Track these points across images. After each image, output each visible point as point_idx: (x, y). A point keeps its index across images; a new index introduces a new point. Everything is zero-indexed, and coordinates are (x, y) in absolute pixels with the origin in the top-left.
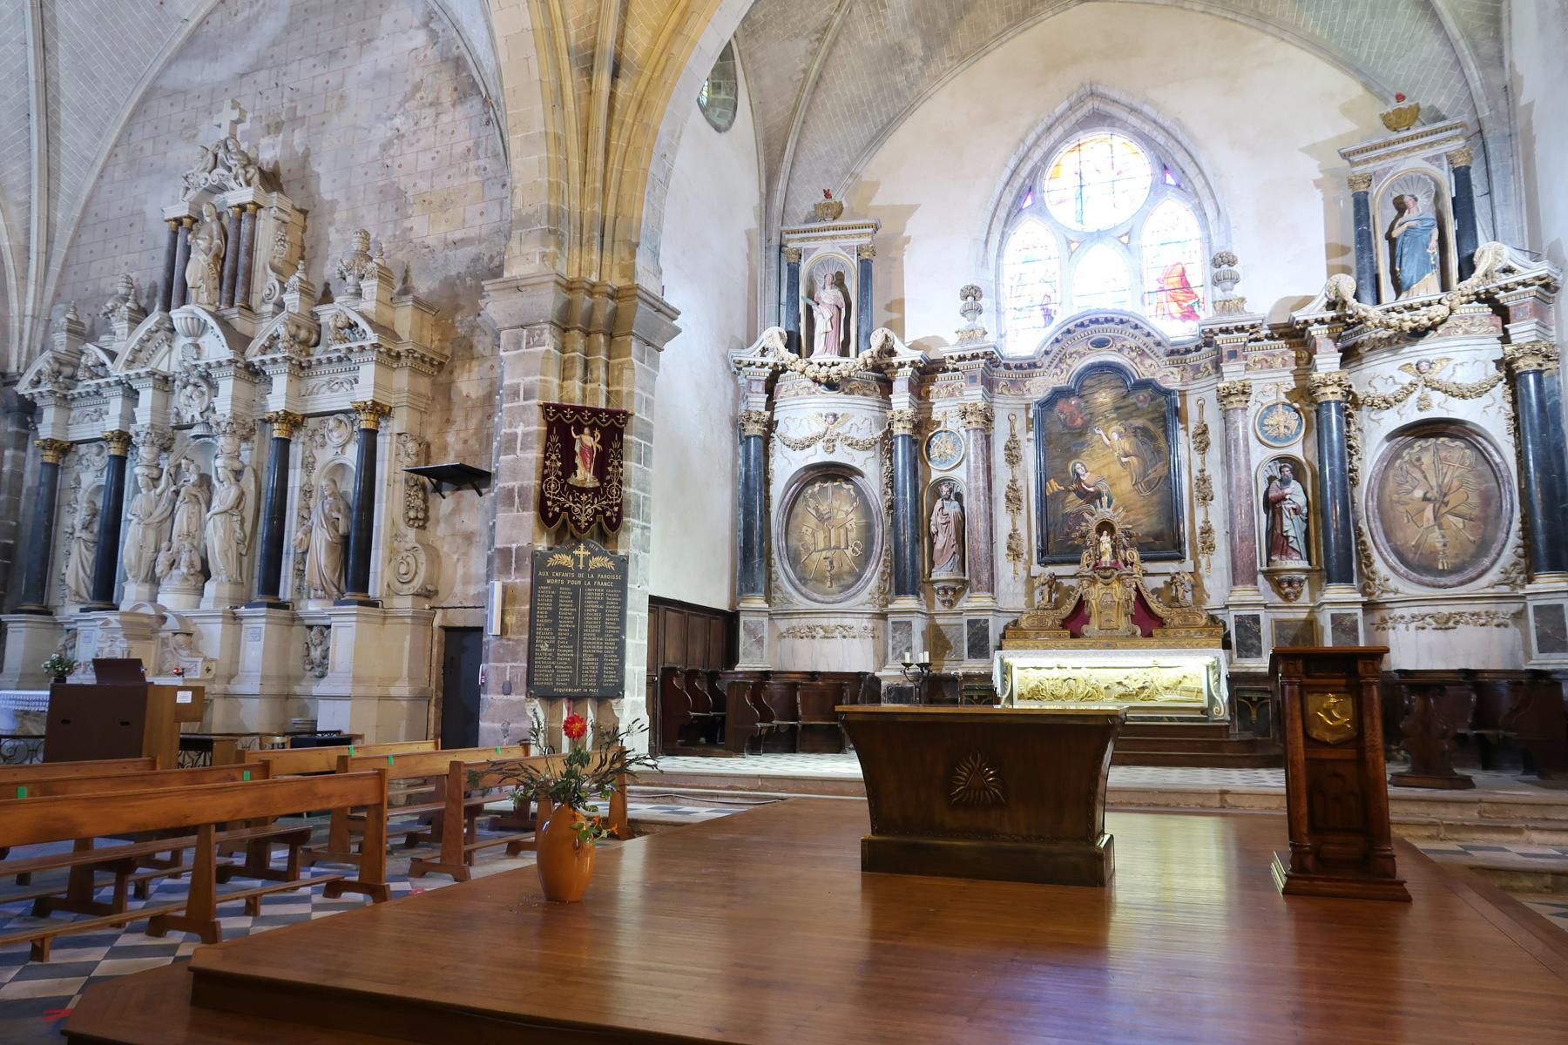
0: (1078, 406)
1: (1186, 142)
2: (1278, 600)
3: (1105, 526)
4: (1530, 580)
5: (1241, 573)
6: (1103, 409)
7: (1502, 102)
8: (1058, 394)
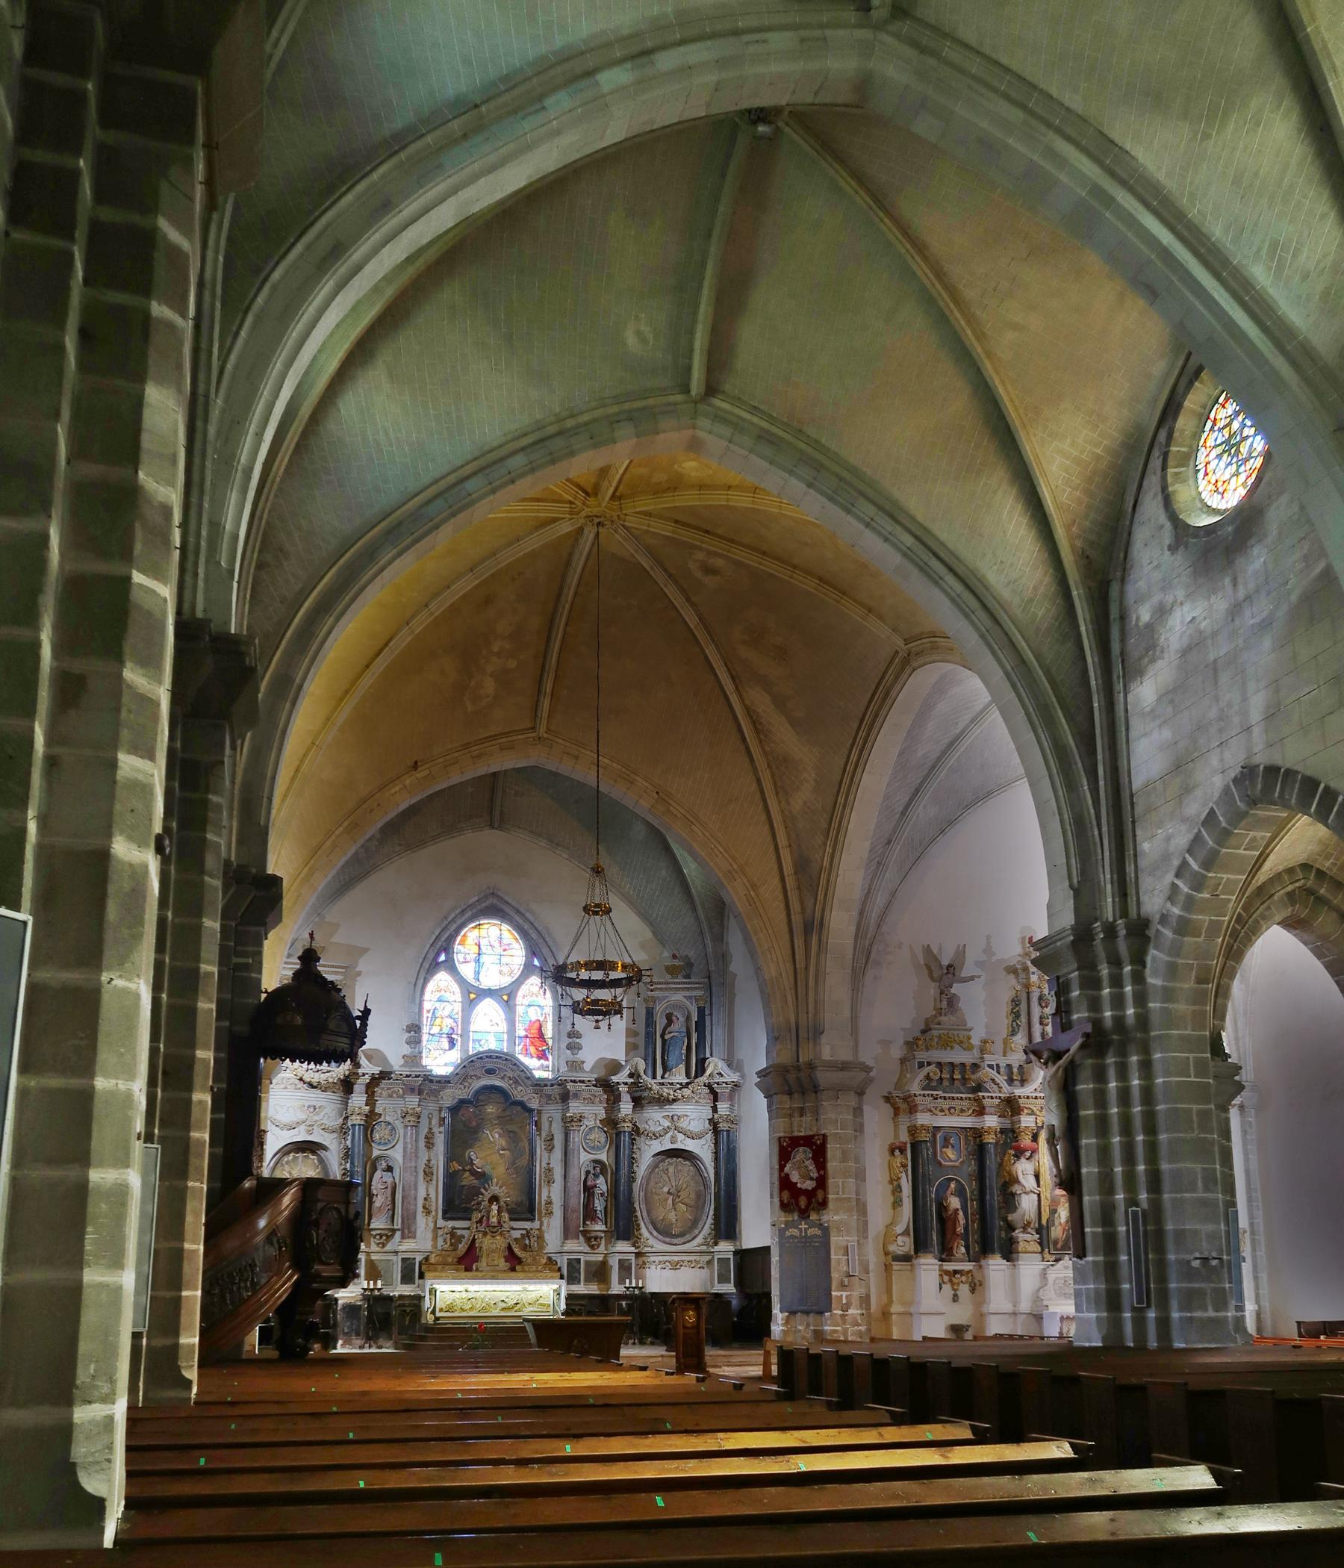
0: (474, 1112)
1: (551, 944)
2: (587, 1249)
3: (494, 1199)
4: (716, 1244)
5: (567, 1233)
6: (490, 1117)
7: (721, 963)
8: (462, 1102)
